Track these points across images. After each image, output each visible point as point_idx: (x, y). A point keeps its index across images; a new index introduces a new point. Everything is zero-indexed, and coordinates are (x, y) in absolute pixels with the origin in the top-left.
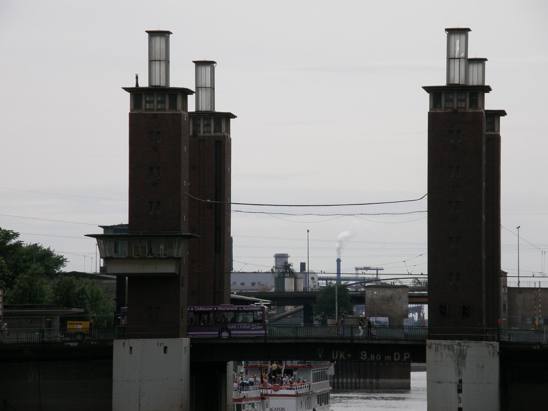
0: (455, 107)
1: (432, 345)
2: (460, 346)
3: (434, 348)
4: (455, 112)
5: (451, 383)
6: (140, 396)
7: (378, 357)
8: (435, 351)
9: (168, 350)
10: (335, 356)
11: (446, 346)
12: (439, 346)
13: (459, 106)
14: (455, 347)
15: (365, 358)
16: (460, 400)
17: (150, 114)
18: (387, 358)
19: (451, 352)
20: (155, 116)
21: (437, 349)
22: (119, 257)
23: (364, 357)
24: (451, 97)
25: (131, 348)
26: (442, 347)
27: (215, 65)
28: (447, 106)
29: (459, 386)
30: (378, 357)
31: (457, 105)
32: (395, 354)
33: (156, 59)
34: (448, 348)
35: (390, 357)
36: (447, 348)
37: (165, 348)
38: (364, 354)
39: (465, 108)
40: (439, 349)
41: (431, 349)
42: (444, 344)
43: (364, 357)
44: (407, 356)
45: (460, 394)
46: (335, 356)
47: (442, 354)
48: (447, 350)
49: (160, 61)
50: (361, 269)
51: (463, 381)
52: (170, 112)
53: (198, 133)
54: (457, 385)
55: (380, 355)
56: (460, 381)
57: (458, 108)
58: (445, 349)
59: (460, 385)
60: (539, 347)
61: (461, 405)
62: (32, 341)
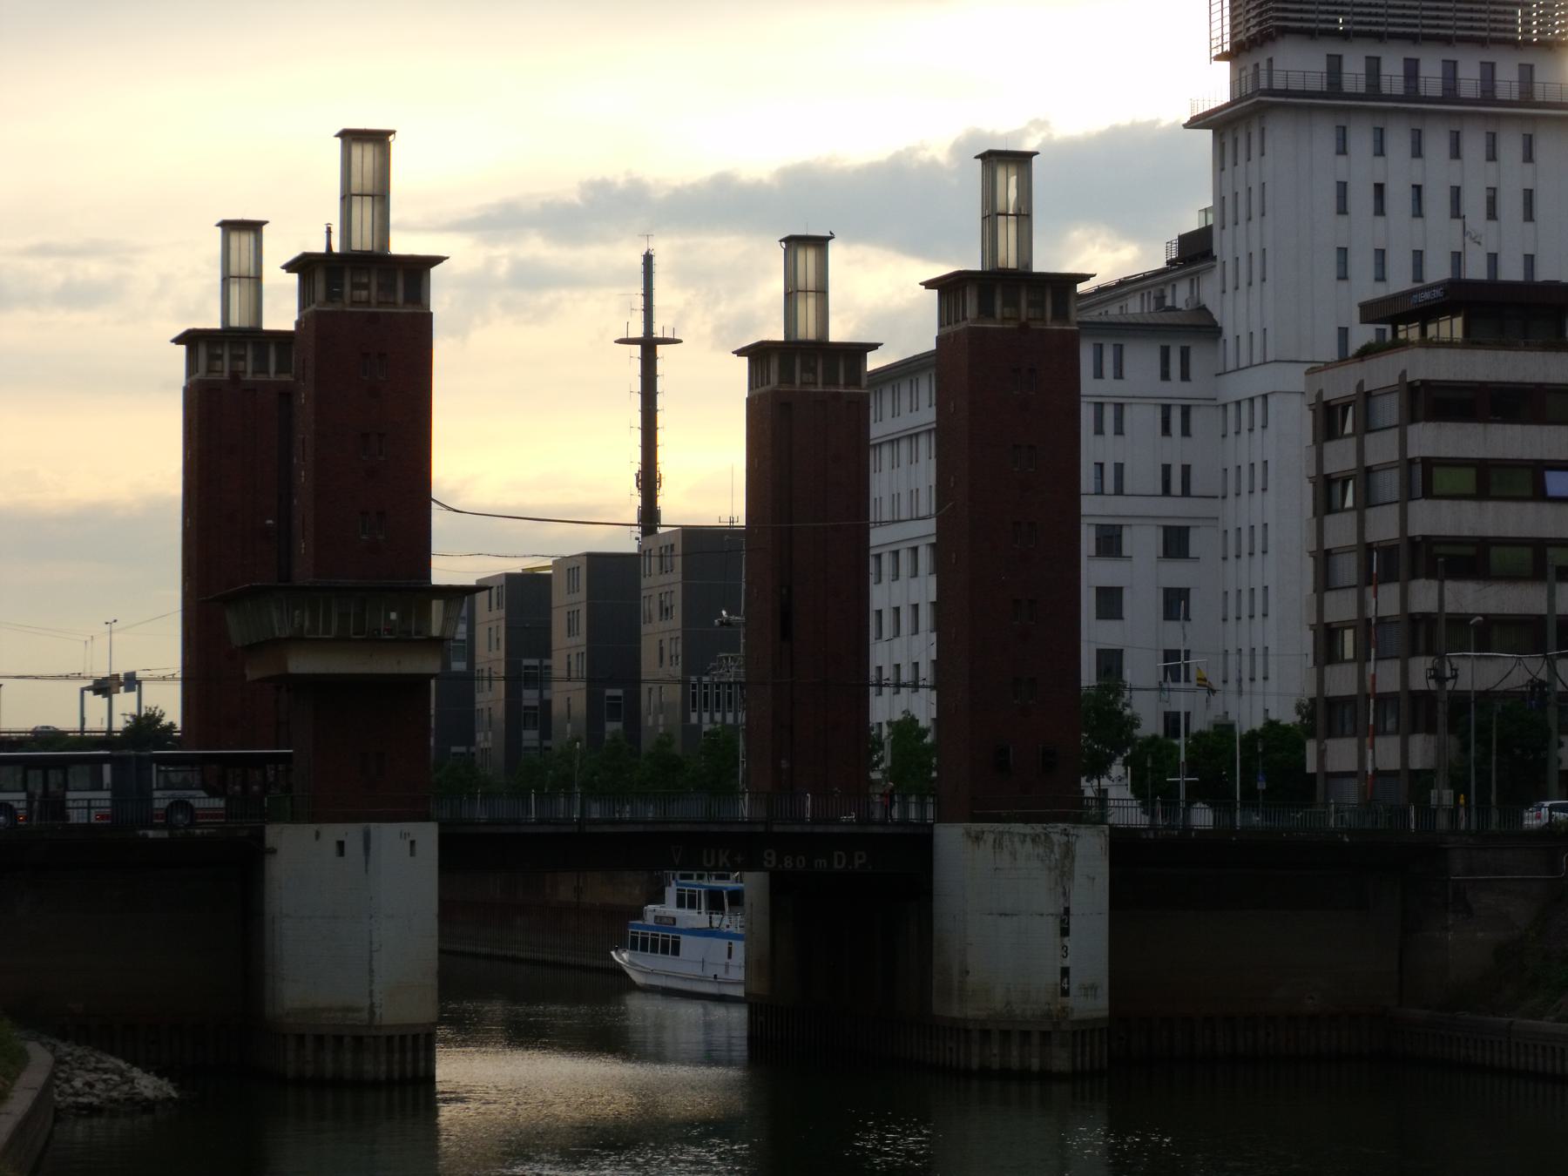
0: (1023, 318)
1: (985, 834)
2: (1067, 835)
3: (992, 840)
4: (1024, 328)
5: (1042, 915)
6: (371, 951)
7: (801, 861)
8: (994, 848)
9: (417, 847)
10: (709, 861)
11: (1025, 835)
12: (1006, 836)
13: (1031, 316)
14: (1056, 838)
15: (774, 863)
16: (1066, 951)
17: (363, 312)
18: (818, 863)
19: (1041, 850)
21: (998, 844)
22: (320, 636)
23: (770, 862)
24: (219, 352)
25: (341, 845)
26: (1016, 839)
27: (391, 138)
28: (1007, 315)
29: (1062, 921)
30: (801, 861)
31: (1003, 313)
32: (836, 854)
33: (365, 192)
34: (1033, 841)
35: (824, 861)
36: (1028, 839)
37: (412, 843)
38: (770, 855)
39: (1043, 319)
40: (1004, 844)
41: (982, 843)
42: (1022, 831)
43: (770, 862)
45: (1066, 939)
46: (709, 861)
47: (1014, 855)
48: (1029, 844)
49: (373, 196)
51: (1072, 911)
52: (405, 311)
53: (241, 374)
54: (1058, 921)
55: (803, 859)
56: (1067, 911)
58: (1023, 842)
59: (1064, 920)
60: (1151, 835)
61: (1067, 963)
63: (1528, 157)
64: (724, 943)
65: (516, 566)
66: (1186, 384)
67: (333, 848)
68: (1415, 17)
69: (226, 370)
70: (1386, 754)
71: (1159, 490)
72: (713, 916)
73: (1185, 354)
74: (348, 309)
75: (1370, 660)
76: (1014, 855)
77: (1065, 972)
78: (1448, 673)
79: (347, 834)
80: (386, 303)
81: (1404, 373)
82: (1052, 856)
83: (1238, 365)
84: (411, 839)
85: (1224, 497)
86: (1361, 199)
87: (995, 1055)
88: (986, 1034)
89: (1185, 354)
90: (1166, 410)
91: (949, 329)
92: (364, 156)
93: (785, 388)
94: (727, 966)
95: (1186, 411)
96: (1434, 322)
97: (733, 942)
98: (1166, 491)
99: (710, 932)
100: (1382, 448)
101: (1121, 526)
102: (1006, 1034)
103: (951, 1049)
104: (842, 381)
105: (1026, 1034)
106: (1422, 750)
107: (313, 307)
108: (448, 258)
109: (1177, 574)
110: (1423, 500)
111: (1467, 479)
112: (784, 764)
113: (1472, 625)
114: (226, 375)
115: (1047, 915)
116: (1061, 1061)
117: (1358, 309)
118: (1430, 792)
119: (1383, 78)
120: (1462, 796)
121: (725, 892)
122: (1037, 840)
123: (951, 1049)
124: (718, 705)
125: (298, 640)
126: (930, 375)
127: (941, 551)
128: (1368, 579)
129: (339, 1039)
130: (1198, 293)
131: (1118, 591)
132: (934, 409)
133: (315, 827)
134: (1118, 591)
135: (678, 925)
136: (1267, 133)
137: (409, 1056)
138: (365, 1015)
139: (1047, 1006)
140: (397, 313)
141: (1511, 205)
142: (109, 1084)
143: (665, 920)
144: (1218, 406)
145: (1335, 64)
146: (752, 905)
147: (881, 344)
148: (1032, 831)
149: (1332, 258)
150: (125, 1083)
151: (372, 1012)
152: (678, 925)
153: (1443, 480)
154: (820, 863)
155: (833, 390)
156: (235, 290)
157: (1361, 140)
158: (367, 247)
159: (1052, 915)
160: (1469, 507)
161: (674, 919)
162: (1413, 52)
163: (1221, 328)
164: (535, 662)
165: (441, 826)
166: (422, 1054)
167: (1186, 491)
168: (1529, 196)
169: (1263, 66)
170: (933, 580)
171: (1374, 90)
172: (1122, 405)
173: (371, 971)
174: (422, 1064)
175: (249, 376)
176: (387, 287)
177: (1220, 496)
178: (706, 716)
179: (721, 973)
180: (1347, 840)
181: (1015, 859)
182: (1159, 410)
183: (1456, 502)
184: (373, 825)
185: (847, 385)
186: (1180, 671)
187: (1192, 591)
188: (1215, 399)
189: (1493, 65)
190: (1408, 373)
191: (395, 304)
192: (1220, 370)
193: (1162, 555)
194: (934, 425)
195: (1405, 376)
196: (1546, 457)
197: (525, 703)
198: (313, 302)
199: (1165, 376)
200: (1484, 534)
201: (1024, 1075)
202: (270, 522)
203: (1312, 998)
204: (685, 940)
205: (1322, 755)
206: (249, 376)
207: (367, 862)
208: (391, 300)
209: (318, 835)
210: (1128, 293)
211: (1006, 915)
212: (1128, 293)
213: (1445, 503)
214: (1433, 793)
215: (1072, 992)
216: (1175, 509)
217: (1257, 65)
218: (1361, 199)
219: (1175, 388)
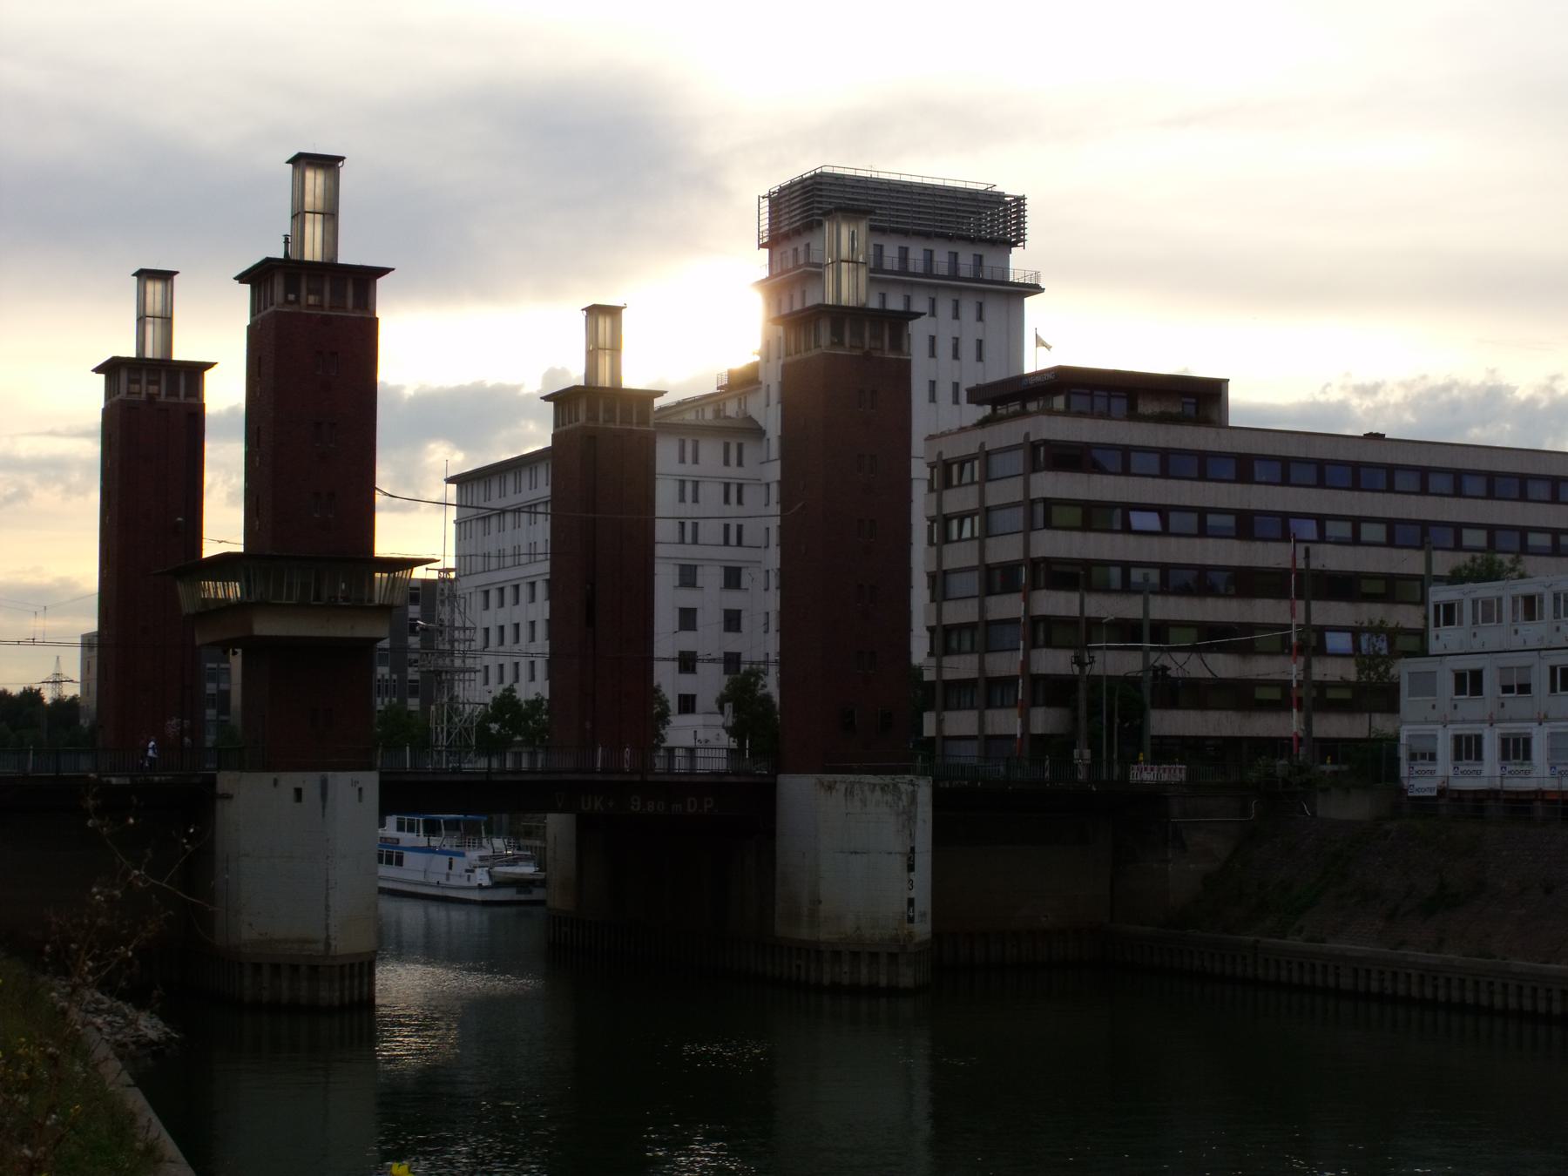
0: (867, 347)
2: (913, 785)
3: (843, 789)
6: (327, 889)
10: (586, 806)
11: (875, 785)
12: (857, 786)
14: (903, 787)
15: (638, 809)
16: (912, 885)
19: (889, 798)
20: (327, 320)
21: (849, 793)
22: (284, 602)
23: (636, 806)
26: (866, 788)
36: (877, 788)
37: (360, 790)
38: (636, 800)
39: (882, 349)
40: (855, 792)
41: (834, 792)
43: (636, 806)
44: (709, 802)
45: (912, 873)
46: (586, 806)
47: (864, 802)
48: (878, 793)
50: (765, 624)
51: (917, 850)
54: (905, 859)
56: (913, 849)
57: (870, 348)
58: (873, 791)
59: (910, 858)
61: (913, 894)
62: (532, 771)
63: (980, 318)
64: (446, 859)
66: (740, 469)
67: (291, 795)
68: (908, 217)
69: (144, 392)
70: (1005, 722)
71: (721, 540)
72: (431, 838)
73: (740, 447)
75: (1019, 649)
76: (864, 802)
77: (911, 902)
78: (1087, 661)
79: (304, 782)
81: (940, 454)
82: (900, 803)
83: (768, 457)
84: (358, 786)
85: (767, 547)
87: (845, 973)
88: (837, 954)
89: (740, 447)
90: (727, 486)
92: (314, 181)
93: (591, 424)
94: (448, 875)
95: (740, 488)
96: (1035, 400)
97: (453, 857)
98: (727, 542)
99: (429, 850)
100: (1004, 492)
101: (696, 566)
102: (855, 955)
103: (799, 967)
105: (874, 956)
106: (1044, 720)
107: (118, 397)
108: (393, 269)
109: (734, 600)
110: (1045, 530)
111: (1075, 515)
112: (588, 725)
113: (1106, 623)
114: (143, 396)
115: (896, 853)
116: (907, 978)
117: (966, 393)
118: (1072, 753)
119: (885, 258)
120: (1329, 758)
121: (442, 821)
122: (886, 788)
123: (799, 967)
124: (387, 693)
126: (547, 465)
127: (555, 587)
128: (988, 589)
129: (295, 968)
130: (745, 406)
131: (694, 611)
132: (549, 488)
133: (273, 775)
134: (694, 611)
135: (401, 844)
136: (807, 293)
137: (356, 983)
138: (321, 947)
139: (895, 932)
140: (348, 317)
142: (114, 1027)
143: (390, 841)
144: (762, 484)
146: (555, 837)
147: (666, 392)
148: (882, 781)
150: (128, 1025)
151: (328, 945)
152: (401, 844)
153: (1059, 515)
155: (629, 427)
156: (149, 329)
158: (318, 258)
159: (900, 853)
160: (1077, 535)
161: (398, 840)
162: (905, 243)
163: (765, 431)
164: (214, 666)
165: (381, 774)
166: (366, 980)
167: (739, 543)
168: (980, 343)
169: (801, 249)
170: (547, 604)
172: (697, 482)
173: (327, 907)
174: (366, 989)
175: (163, 398)
177: (763, 546)
179: (443, 880)
180: (1094, 789)
181: (865, 806)
182: (722, 487)
183: (1068, 533)
186: (1534, 602)
187: (743, 612)
188: (759, 480)
190: (986, 444)
191: (321, 306)
192: (765, 460)
193: (723, 586)
194: (549, 498)
195: (1029, 437)
196: (1131, 500)
197: (208, 692)
198: (272, 304)
199: (727, 463)
200: (1088, 557)
202: (180, 519)
203: (1046, 916)
204: (407, 856)
205: (940, 722)
206: (163, 398)
207: (324, 807)
209: (276, 782)
210: (686, 409)
211: (856, 853)
212: (686, 409)
213: (1060, 533)
214: (1076, 752)
215: (916, 919)
216: (733, 555)
217: (796, 250)
219: (733, 472)
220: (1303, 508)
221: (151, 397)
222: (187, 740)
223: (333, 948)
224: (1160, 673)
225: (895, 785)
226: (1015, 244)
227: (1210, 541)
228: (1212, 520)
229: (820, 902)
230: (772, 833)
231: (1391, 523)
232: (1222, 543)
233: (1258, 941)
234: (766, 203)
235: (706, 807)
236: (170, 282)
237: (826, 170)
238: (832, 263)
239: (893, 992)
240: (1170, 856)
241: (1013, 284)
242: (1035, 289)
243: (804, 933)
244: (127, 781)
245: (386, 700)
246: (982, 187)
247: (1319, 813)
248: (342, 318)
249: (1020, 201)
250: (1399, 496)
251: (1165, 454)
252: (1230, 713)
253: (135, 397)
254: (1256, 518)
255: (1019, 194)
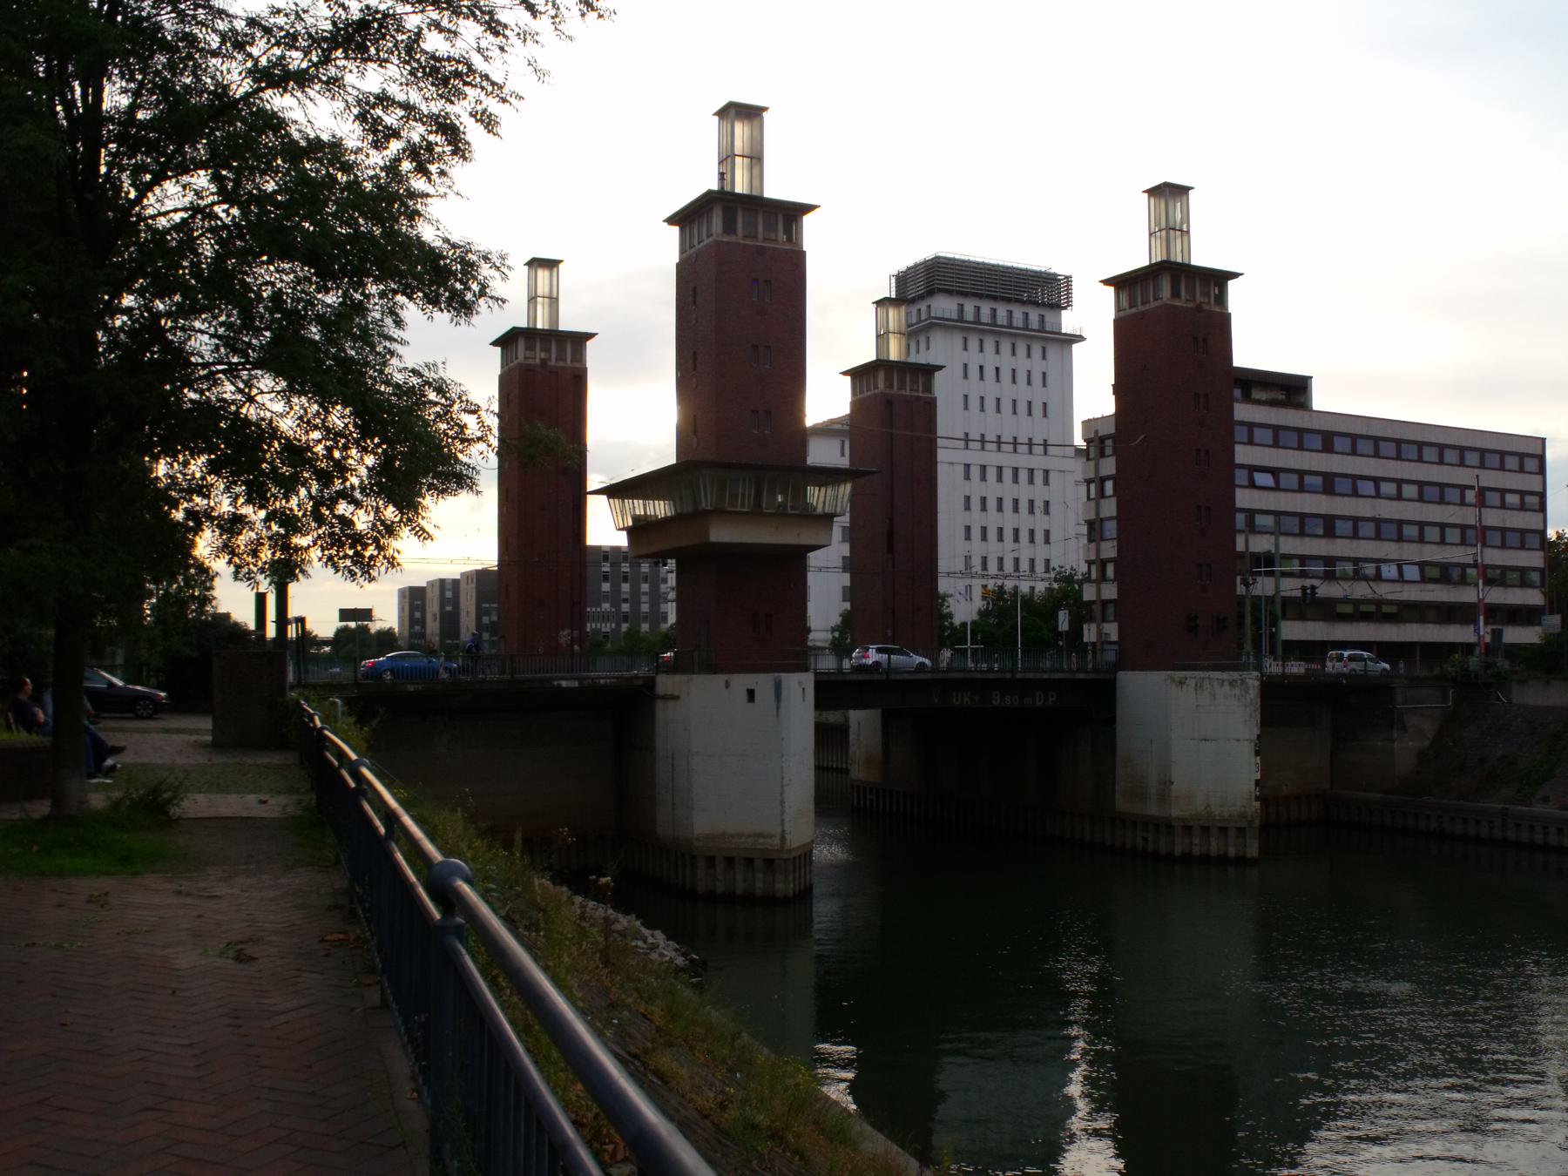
0: (1198, 302)
3: (1193, 685)
4: (1199, 308)
5: (1238, 740)
6: (782, 786)
11: (1223, 681)
19: (1237, 691)
21: (1199, 687)
22: (739, 509)
26: (1216, 683)
36: (1226, 683)
39: (1209, 303)
41: (1185, 687)
42: (1221, 677)
47: (1214, 696)
48: (1227, 687)
54: (1253, 745)
58: (1222, 685)
63: (1044, 357)
65: (479, 567)
67: (744, 695)
69: (538, 357)
74: (742, 242)
76: (1214, 696)
80: (769, 240)
86: (974, 372)
88: (1188, 829)
91: (1122, 313)
93: (888, 391)
98: (1046, 472)
102: (1206, 830)
103: (1145, 839)
104: (921, 389)
105: (1223, 830)
114: (538, 361)
123: (1145, 839)
125: (719, 512)
129: (749, 861)
133: (722, 678)
136: (931, 339)
138: (777, 841)
141: (1037, 379)
145: (961, 306)
149: (961, 399)
151: (783, 838)
154: (1028, 701)
155: (916, 394)
157: (973, 343)
158: (746, 191)
162: (995, 305)
171: (978, 321)
173: (782, 803)
175: (553, 362)
176: (771, 227)
178: (604, 625)
184: (783, 676)
185: (923, 392)
189: (1027, 314)
201: (1206, 860)
206: (553, 362)
207: (778, 709)
208: (774, 238)
209: (727, 685)
217: (920, 310)
218: (974, 372)
220: (1366, 473)
221: (544, 362)
222: (576, 647)
223: (788, 842)
224: (1309, 591)
225: (1243, 681)
226: (1065, 308)
227: (1307, 495)
228: (1307, 479)
229: (1172, 783)
230: (1112, 720)
231: (1421, 484)
232: (1314, 496)
233: (1507, 809)
234: (893, 280)
235: (1051, 699)
236: (555, 270)
237: (941, 254)
238: (1160, 230)
239: (1242, 861)
240: (1395, 735)
241: (1066, 334)
242: (1080, 338)
243: (1153, 810)
244: (576, 684)
245: (608, 625)
246: (1043, 270)
247: (1514, 701)
248: (774, 249)
249: (1068, 279)
250: (1426, 465)
251: (1277, 429)
252: (1321, 623)
253: (531, 361)
254: (1337, 479)
255: (1068, 274)
